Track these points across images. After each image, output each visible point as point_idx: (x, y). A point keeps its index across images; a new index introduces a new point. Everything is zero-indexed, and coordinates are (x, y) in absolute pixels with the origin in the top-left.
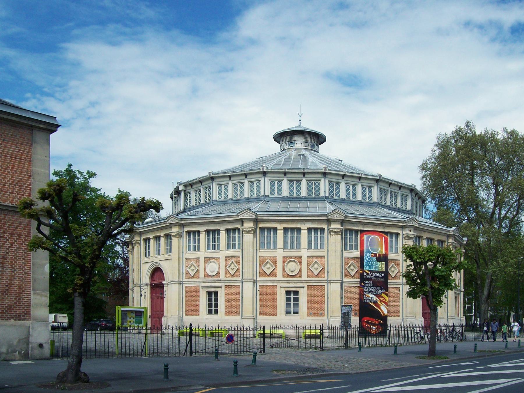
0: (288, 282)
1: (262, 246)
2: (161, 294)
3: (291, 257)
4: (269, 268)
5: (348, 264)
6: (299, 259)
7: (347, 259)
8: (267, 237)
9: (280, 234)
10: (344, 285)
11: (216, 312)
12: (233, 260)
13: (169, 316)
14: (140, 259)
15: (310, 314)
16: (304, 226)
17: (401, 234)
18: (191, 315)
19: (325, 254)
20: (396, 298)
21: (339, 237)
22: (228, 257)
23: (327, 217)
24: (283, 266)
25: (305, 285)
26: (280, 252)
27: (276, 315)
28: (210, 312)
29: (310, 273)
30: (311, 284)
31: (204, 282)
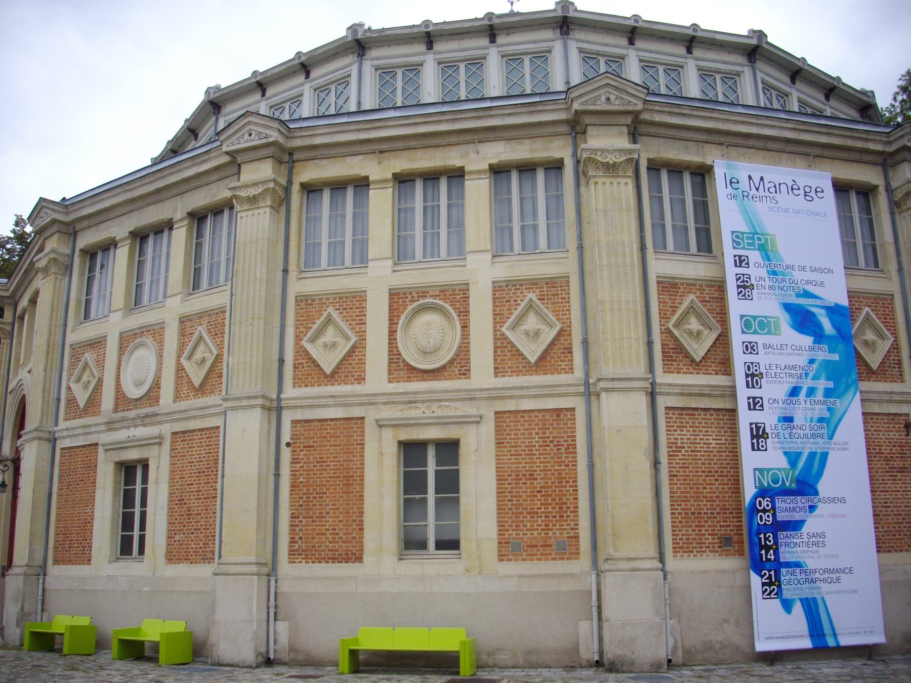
1: (310, 262)
4: (334, 345)
5: (674, 309)
7: (669, 286)
10: (662, 402)
15: (508, 549)
16: (478, 158)
17: (881, 189)
19: (570, 266)
20: (898, 464)
21: (625, 189)
24: (392, 333)
26: (378, 278)
27: (359, 559)
29: (507, 357)
30: (510, 406)
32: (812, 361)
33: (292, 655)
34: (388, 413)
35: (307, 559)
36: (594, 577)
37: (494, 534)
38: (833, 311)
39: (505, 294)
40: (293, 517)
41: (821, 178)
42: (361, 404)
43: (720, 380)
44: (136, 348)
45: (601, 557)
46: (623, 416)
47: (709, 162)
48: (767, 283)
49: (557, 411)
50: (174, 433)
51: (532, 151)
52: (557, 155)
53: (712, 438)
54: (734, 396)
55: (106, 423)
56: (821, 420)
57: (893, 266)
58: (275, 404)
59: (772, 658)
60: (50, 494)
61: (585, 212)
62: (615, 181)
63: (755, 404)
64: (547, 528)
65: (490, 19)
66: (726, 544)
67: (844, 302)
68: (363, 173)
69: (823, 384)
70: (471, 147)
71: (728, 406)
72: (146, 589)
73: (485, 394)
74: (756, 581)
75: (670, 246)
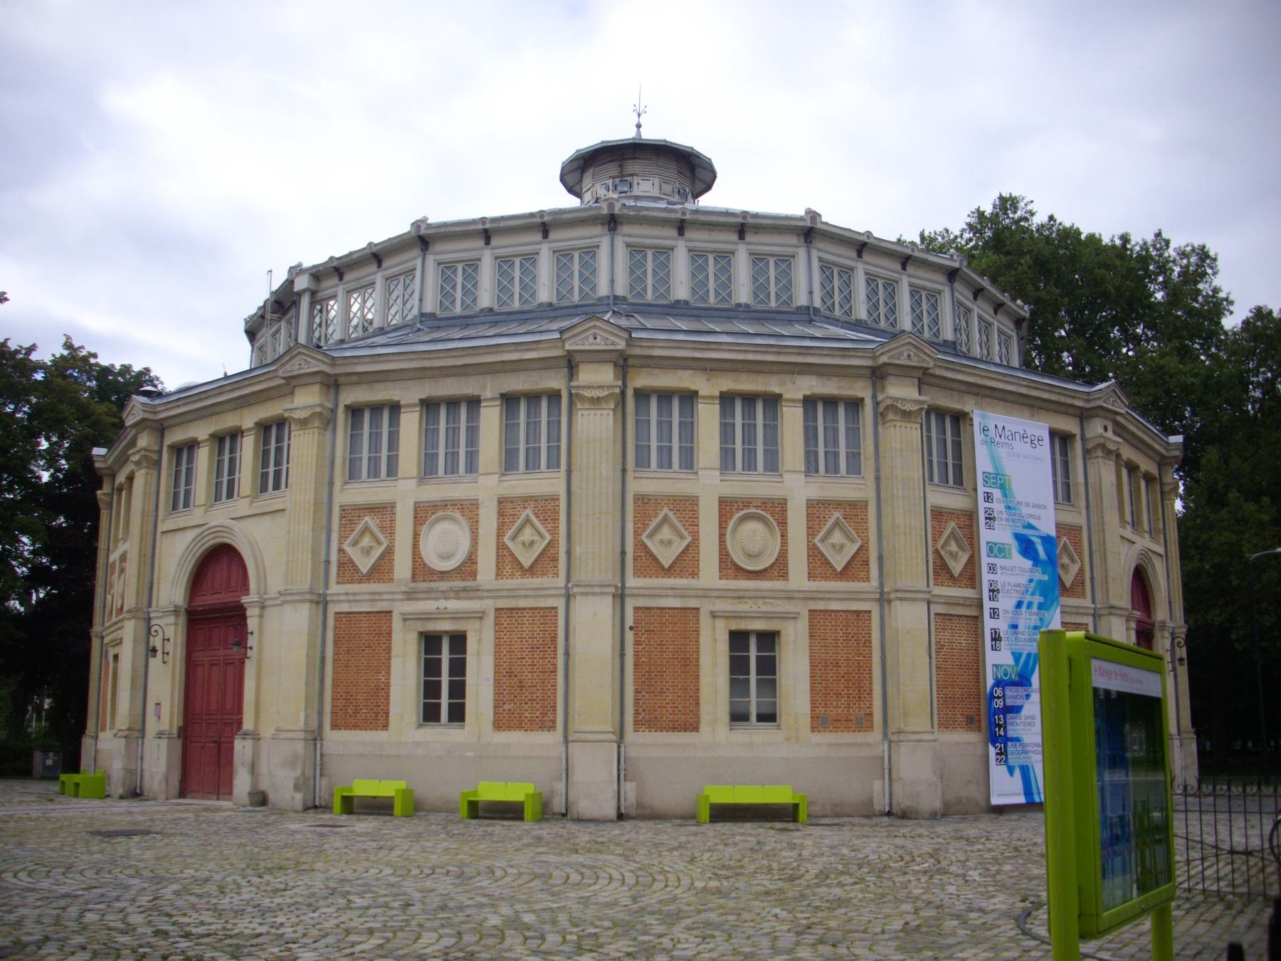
0: (740, 596)
2: (238, 644)
3: (747, 503)
4: (670, 542)
6: (776, 510)
8: (660, 423)
9: (708, 416)
11: (458, 714)
12: (529, 512)
13: (267, 731)
14: (152, 519)
15: (819, 723)
17: (1078, 437)
18: (356, 727)
19: (868, 493)
22: (511, 500)
23: (874, 358)
24: (722, 536)
25: (803, 609)
26: (709, 483)
28: (430, 714)
29: (818, 564)
30: (821, 606)
31: (410, 596)
32: (1031, 581)
33: (639, 811)
34: (720, 606)
35: (650, 728)
36: (886, 746)
37: (809, 711)
38: (1047, 540)
39: (816, 509)
40: (637, 691)
41: (1039, 428)
42: (697, 597)
43: (968, 593)
44: (445, 518)
45: (891, 729)
46: (910, 621)
47: (967, 409)
48: (1004, 516)
49: (857, 613)
50: (497, 610)
51: (839, 388)
52: (860, 394)
53: (963, 639)
54: (981, 606)
55: (404, 593)
56: (1035, 628)
57: (1083, 504)
58: (620, 591)
59: (1000, 810)
60: (323, 659)
61: (881, 448)
62: (909, 425)
63: (994, 614)
64: (848, 707)
65: (744, 217)
66: (971, 722)
67: (1053, 533)
68: (693, 387)
69: (1037, 599)
70: (787, 378)
71: (974, 613)
72: (470, 754)
73: (802, 595)
74: (992, 751)
75: (936, 479)
